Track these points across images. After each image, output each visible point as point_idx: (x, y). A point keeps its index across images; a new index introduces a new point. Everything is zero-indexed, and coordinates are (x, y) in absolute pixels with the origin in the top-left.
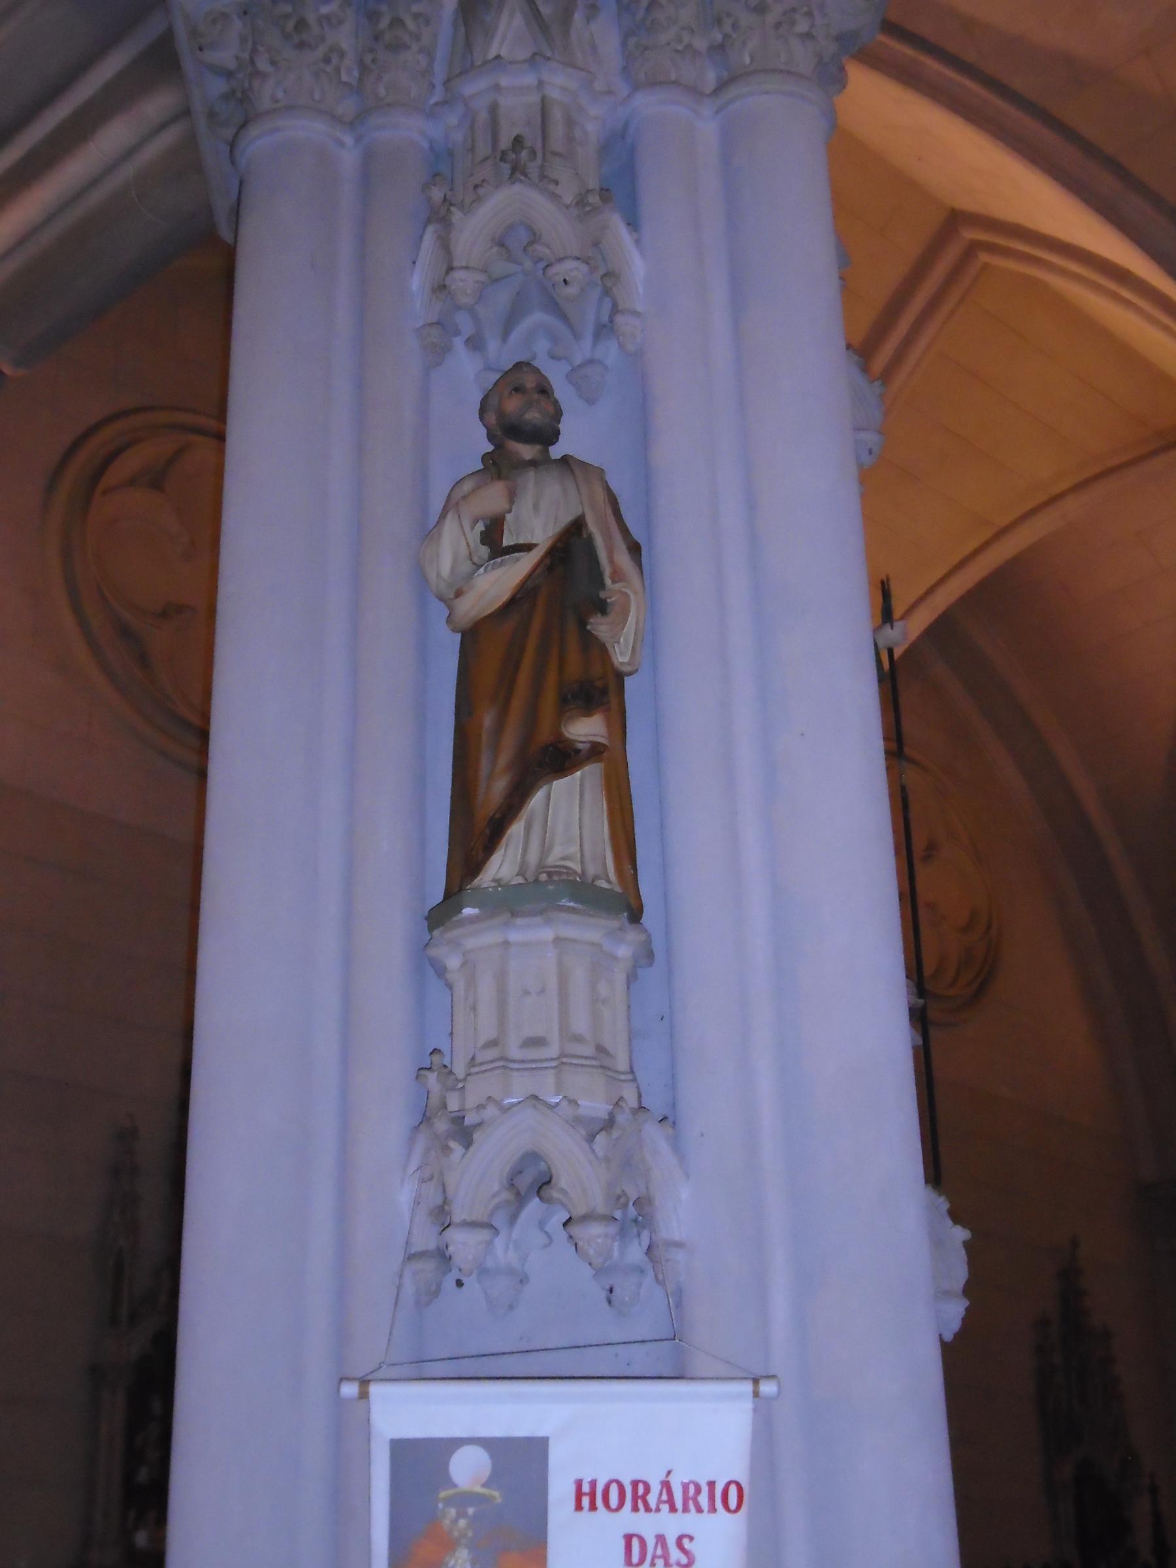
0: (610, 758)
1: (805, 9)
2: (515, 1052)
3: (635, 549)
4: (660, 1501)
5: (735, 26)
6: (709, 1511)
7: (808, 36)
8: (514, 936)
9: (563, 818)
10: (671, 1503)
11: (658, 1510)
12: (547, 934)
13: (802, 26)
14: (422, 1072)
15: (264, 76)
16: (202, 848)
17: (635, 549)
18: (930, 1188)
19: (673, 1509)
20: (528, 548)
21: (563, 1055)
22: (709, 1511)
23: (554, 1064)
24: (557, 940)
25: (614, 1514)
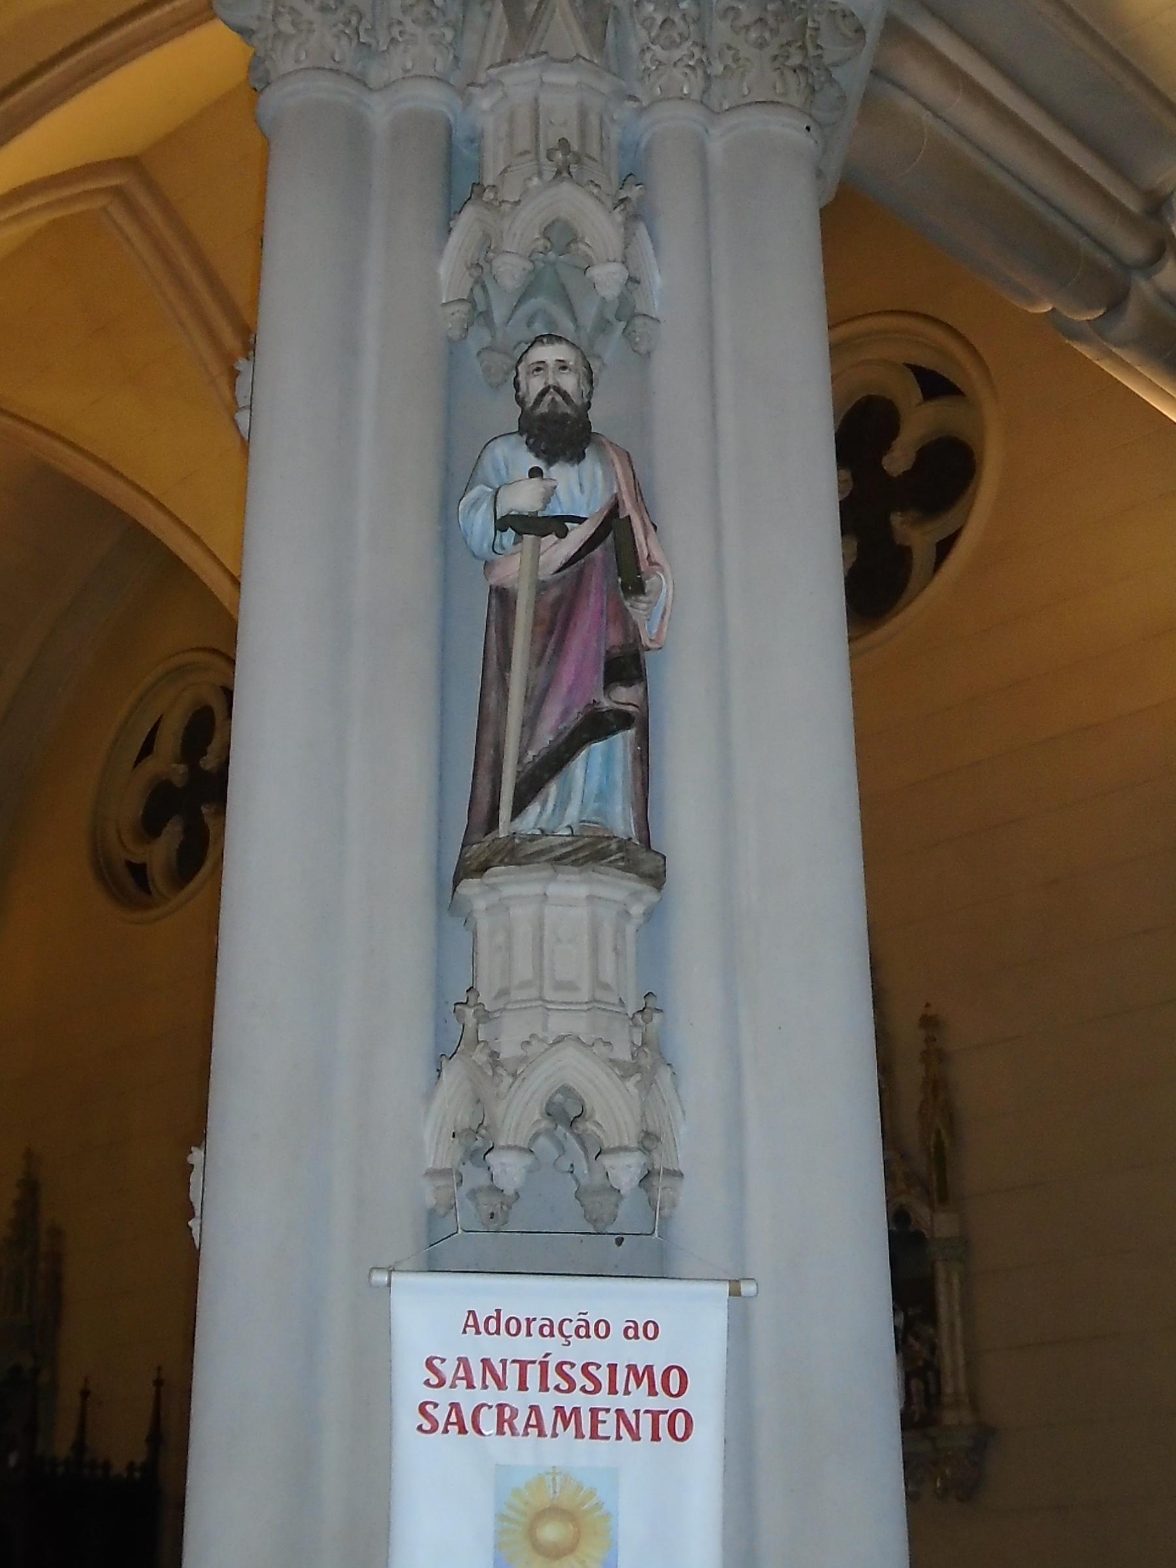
0: (636, 721)
1: (799, 44)
2: (549, 994)
3: (655, 528)
4: (528, 1425)
5: (736, 59)
6: (592, 1437)
7: (802, 68)
8: (553, 889)
9: (594, 781)
10: (539, 1426)
11: (526, 1434)
12: (581, 891)
13: (796, 60)
14: (458, 1007)
15: (287, 38)
16: (908, 1422)
17: (655, 528)
18: (889, 397)
19: (541, 1434)
20: (559, 525)
21: (594, 1000)
22: (592, 1437)
23: (585, 1007)
24: (590, 898)
25: (424, 1435)
